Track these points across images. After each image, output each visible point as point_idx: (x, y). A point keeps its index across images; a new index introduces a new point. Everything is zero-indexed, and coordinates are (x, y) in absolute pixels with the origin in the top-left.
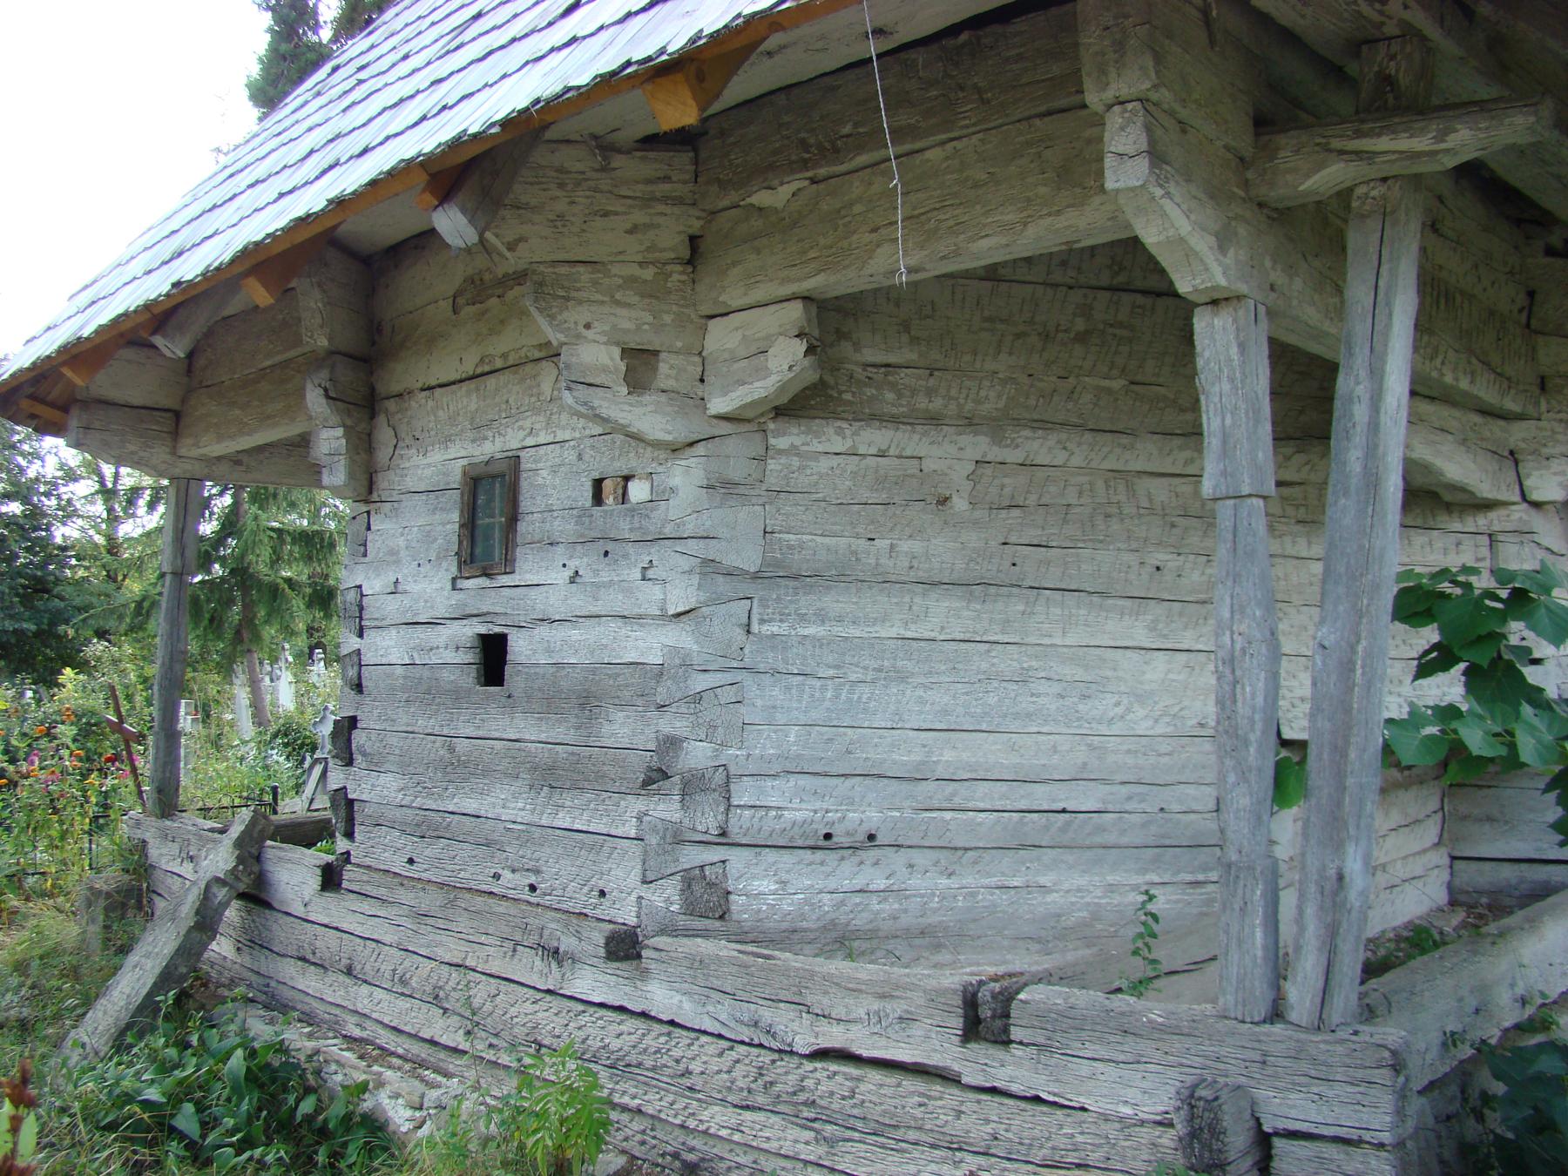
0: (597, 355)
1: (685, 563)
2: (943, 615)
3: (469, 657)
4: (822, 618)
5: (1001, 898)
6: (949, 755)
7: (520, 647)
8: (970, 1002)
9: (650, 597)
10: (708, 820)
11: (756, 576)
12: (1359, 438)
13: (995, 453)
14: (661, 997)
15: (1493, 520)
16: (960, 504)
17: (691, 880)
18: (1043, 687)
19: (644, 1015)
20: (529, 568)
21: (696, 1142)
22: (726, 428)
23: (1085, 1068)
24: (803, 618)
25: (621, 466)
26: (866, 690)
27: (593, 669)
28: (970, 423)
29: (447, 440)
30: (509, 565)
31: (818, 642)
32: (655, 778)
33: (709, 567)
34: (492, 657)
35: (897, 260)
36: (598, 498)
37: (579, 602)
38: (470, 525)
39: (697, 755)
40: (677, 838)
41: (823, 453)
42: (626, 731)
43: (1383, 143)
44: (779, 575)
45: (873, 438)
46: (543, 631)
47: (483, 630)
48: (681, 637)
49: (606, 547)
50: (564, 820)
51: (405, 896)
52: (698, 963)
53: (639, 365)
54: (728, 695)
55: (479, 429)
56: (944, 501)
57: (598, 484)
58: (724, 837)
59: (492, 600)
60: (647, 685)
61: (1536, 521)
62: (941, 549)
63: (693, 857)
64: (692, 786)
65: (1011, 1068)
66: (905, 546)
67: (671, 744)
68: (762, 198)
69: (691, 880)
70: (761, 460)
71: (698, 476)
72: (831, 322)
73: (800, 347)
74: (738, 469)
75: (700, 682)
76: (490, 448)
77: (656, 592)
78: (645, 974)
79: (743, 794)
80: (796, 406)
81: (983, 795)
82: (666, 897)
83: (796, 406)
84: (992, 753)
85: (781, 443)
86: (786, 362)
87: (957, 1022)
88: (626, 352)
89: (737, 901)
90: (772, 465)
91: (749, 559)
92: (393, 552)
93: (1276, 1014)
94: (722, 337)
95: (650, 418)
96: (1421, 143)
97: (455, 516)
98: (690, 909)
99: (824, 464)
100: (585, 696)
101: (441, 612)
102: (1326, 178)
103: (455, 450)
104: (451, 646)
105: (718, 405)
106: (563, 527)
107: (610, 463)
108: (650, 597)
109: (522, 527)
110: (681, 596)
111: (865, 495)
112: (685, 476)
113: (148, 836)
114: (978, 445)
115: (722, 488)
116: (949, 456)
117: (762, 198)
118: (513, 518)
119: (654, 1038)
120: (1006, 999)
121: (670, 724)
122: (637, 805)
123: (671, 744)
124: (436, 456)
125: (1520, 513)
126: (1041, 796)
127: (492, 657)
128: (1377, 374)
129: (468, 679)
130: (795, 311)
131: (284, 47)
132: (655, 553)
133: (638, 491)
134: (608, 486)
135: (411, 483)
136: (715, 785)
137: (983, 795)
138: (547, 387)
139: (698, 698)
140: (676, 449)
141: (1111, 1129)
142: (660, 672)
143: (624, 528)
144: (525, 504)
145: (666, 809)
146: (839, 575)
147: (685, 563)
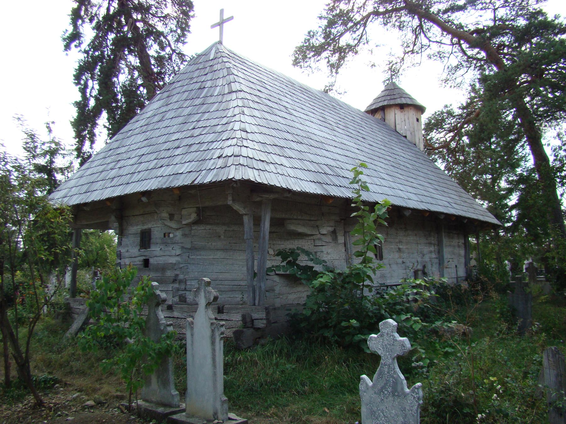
0: (165, 215)
1: (179, 247)
2: (219, 255)
4: (200, 255)
5: (229, 299)
6: (221, 276)
7: (152, 261)
8: (219, 308)
9: (173, 252)
10: (183, 287)
11: (190, 249)
12: (262, 232)
13: (228, 229)
14: (176, 314)
15: (314, 237)
16: (222, 237)
17: (180, 296)
18: (236, 266)
19: (173, 317)
20: (153, 248)
21: (181, 336)
22: (184, 226)
23: (232, 314)
24: (197, 255)
25: (169, 231)
26: (207, 267)
27: (164, 264)
28: (224, 224)
29: (137, 225)
30: (149, 247)
31: (200, 259)
32: (174, 281)
33: (183, 248)
34: (146, 263)
35: (207, 204)
36: (165, 236)
37: (162, 253)
38: (142, 240)
39: (181, 277)
40: (178, 290)
41: (201, 229)
42: (169, 274)
43: (264, 196)
44: (194, 249)
45: (208, 227)
46: (155, 258)
48: (178, 259)
49: (166, 244)
52: (181, 308)
53: (171, 217)
54: (186, 267)
55: (143, 224)
56: (220, 237)
57: (165, 234)
58: (185, 289)
59: (147, 253)
60: (173, 266)
61: (322, 237)
62: (219, 244)
63: (181, 293)
64: (181, 282)
65: (224, 316)
66: (213, 244)
67: (177, 275)
68: (190, 192)
69: (180, 296)
70: (191, 231)
71: (181, 233)
72: (199, 211)
73: (196, 215)
74: (187, 232)
75: (181, 266)
76: (146, 227)
77: (174, 252)
78: (173, 311)
79: (188, 283)
80: (195, 223)
81: (226, 283)
82: (176, 299)
83: (195, 223)
84: (227, 276)
85: (194, 228)
86: (194, 216)
87: (217, 311)
88: (170, 214)
89: (188, 299)
90: (192, 231)
91: (189, 246)
92: (127, 245)
93: (254, 305)
94: (184, 212)
95: (173, 225)
96: (267, 196)
97: (139, 239)
98: (180, 301)
99: (201, 231)
100: (163, 268)
102: (258, 199)
103: (139, 227)
104: (139, 261)
105: (184, 222)
106: (159, 241)
107: (166, 230)
108: (173, 252)
109: (151, 241)
110: (178, 252)
111: (207, 236)
112: (179, 233)
113: (70, 302)
114: (225, 228)
115: (185, 235)
116: (220, 229)
117: (190, 192)
118: (150, 239)
119: (175, 320)
120: (223, 307)
121: (177, 272)
122: (172, 285)
123: (177, 275)
124: (135, 228)
125: (319, 236)
126: (236, 283)
127: (146, 263)
128: (264, 224)
129: (142, 267)
130: (195, 209)
131: (82, 118)
132: (174, 245)
133: (171, 235)
134: (166, 234)
135: (130, 232)
136: (184, 281)
137: (226, 283)
138: (156, 218)
139: (181, 268)
140: (177, 229)
141: (236, 322)
142: (175, 264)
143: (169, 241)
144: (152, 237)
145: (176, 285)
146: (203, 248)
147: (179, 247)
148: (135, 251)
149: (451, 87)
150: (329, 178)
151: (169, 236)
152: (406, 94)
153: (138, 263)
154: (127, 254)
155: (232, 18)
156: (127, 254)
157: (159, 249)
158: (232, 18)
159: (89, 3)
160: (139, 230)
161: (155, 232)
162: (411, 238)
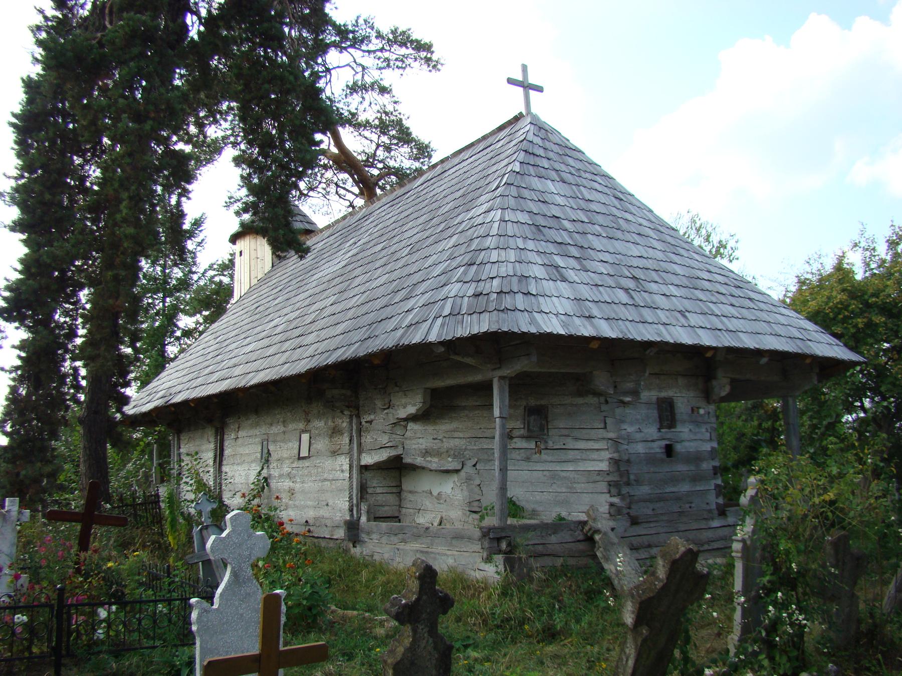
3: (664, 450)
7: (678, 448)
25: (697, 405)
34: (669, 450)
37: (693, 437)
47: (668, 443)
50: (698, 488)
51: (665, 518)
55: (660, 389)
101: (655, 438)
104: (657, 447)
127: (669, 450)
129: (664, 456)
148: (651, 431)
149: (395, 103)
150: (721, 322)
151: (698, 413)
152: (591, 163)
153: (658, 450)
154: (638, 436)
155: (524, 68)
156: (638, 436)
157: (687, 430)
158: (524, 68)
159: (318, 20)
160: (654, 399)
161: (679, 405)
162: (232, 387)
